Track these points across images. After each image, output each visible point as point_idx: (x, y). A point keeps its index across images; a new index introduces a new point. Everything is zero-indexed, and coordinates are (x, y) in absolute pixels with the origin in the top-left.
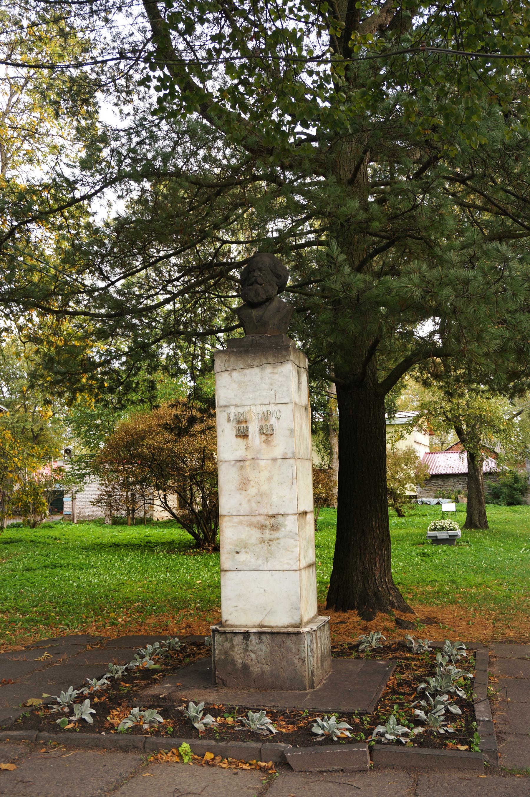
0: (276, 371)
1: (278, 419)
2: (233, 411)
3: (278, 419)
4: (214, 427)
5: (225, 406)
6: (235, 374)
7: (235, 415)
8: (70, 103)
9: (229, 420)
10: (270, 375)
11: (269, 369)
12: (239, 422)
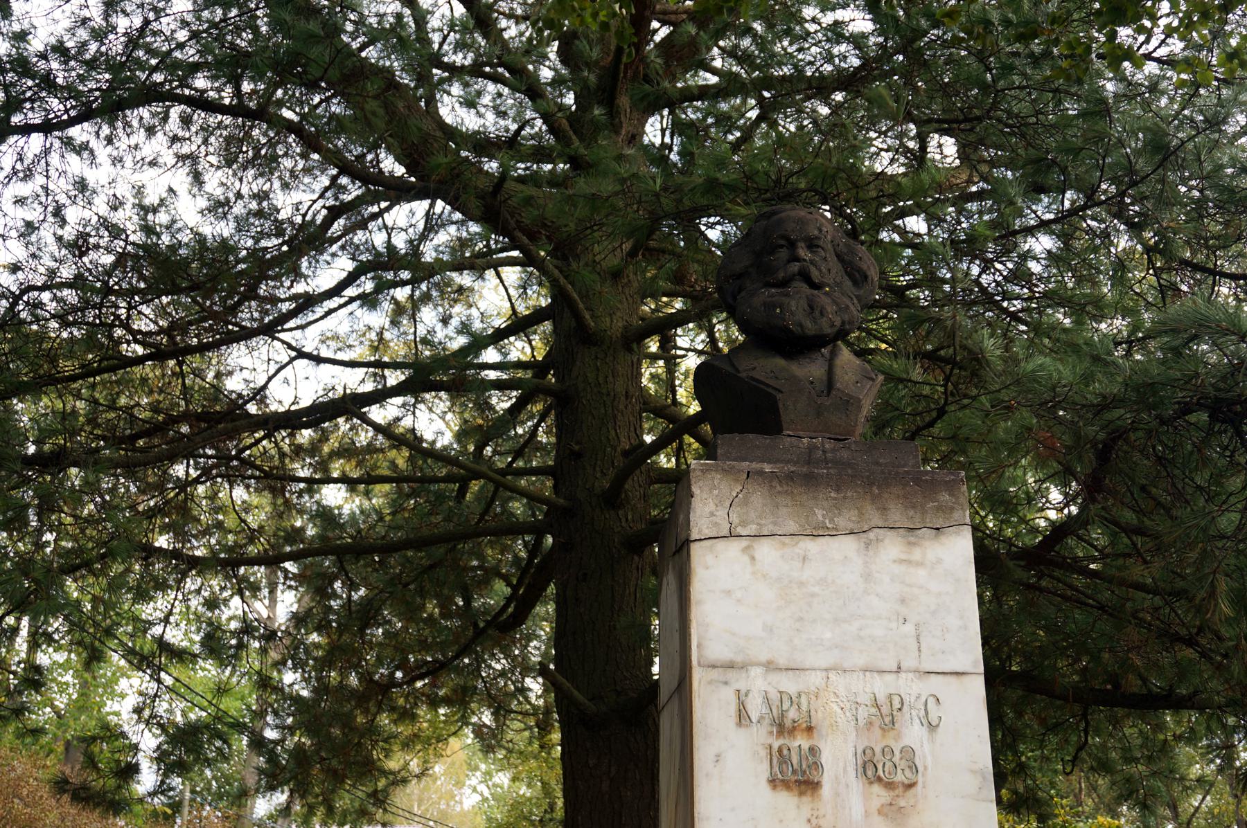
0: (917, 554)
5: (730, 666)
6: (767, 551)
9: (742, 716)
12: (782, 728)
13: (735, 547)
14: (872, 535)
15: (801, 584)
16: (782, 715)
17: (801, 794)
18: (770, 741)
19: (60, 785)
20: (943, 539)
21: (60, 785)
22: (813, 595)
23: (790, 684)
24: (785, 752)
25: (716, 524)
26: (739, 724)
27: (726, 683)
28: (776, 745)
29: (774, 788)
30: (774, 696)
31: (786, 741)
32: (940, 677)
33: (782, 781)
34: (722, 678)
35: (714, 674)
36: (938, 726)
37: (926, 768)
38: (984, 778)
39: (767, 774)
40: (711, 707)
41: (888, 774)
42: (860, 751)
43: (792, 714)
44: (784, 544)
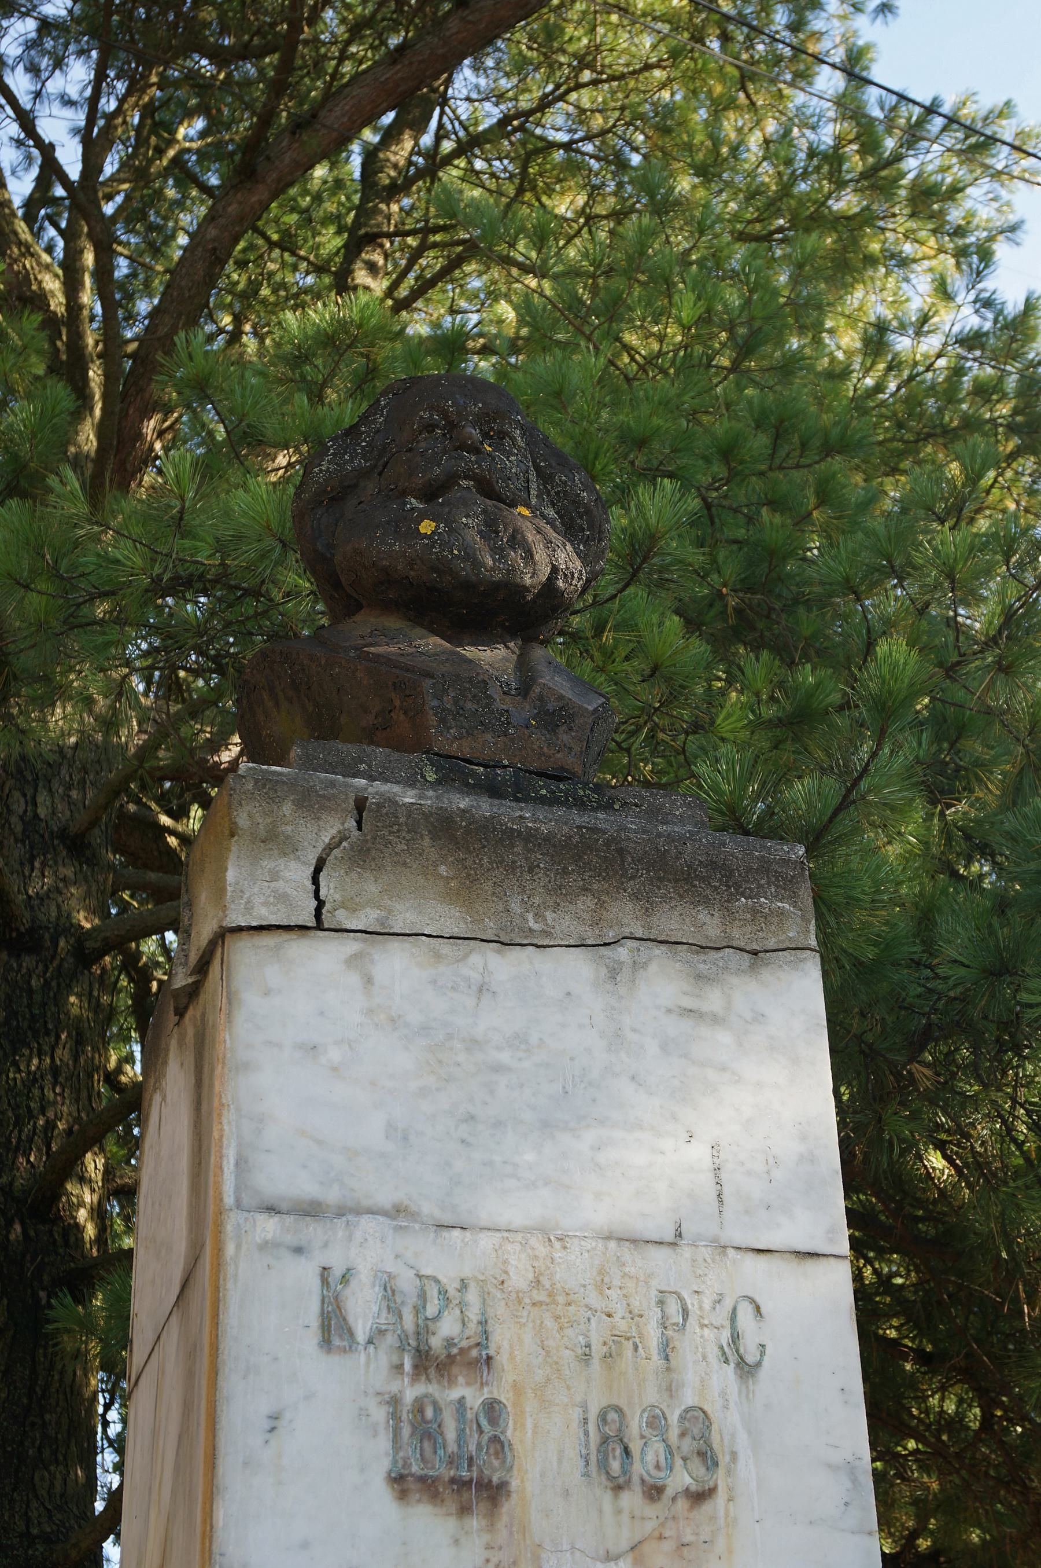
0: (713, 1000)
5: (310, 1210)
6: (397, 966)
7: (389, 1292)
9: (333, 1328)
12: (428, 1361)
13: (325, 955)
14: (623, 952)
15: (473, 1044)
16: (423, 1331)
17: (464, 1510)
18: (394, 1387)
19: (325, 1271)
20: (766, 974)
21: (325, 1271)
22: (498, 1068)
23: (445, 1261)
24: (429, 1413)
25: (282, 898)
26: (326, 1343)
27: (298, 1250)
28: (410, 1394)
29: (403, 1495)
30: (406, 1282)
31: (432, 1389)
32: (762, 1259)
33: (422, 1479)
34: (288, 1238)
35: (268, 1227)
36: (759, 1364)
37: (734, 1455)
38: (854, 1481)
39: (382, 1466)
40: (267, 1304)
41: (664, 1467)
42: (593, 1416)
43: (448, 1327)
44: (438, 956)
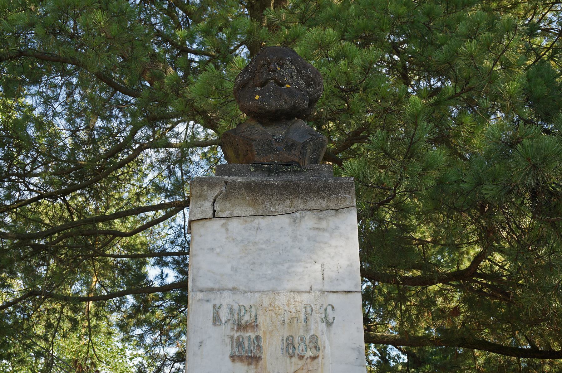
0: (324, 224)
1: (329, 324)
2: (226, 300)
3: (329, 324)
4: (260, 358)
6: (234, 224)
7: (231, 309)
8: (131, 299)
9: (216, 320)
10: (312, 233)
11: (309, 221)
